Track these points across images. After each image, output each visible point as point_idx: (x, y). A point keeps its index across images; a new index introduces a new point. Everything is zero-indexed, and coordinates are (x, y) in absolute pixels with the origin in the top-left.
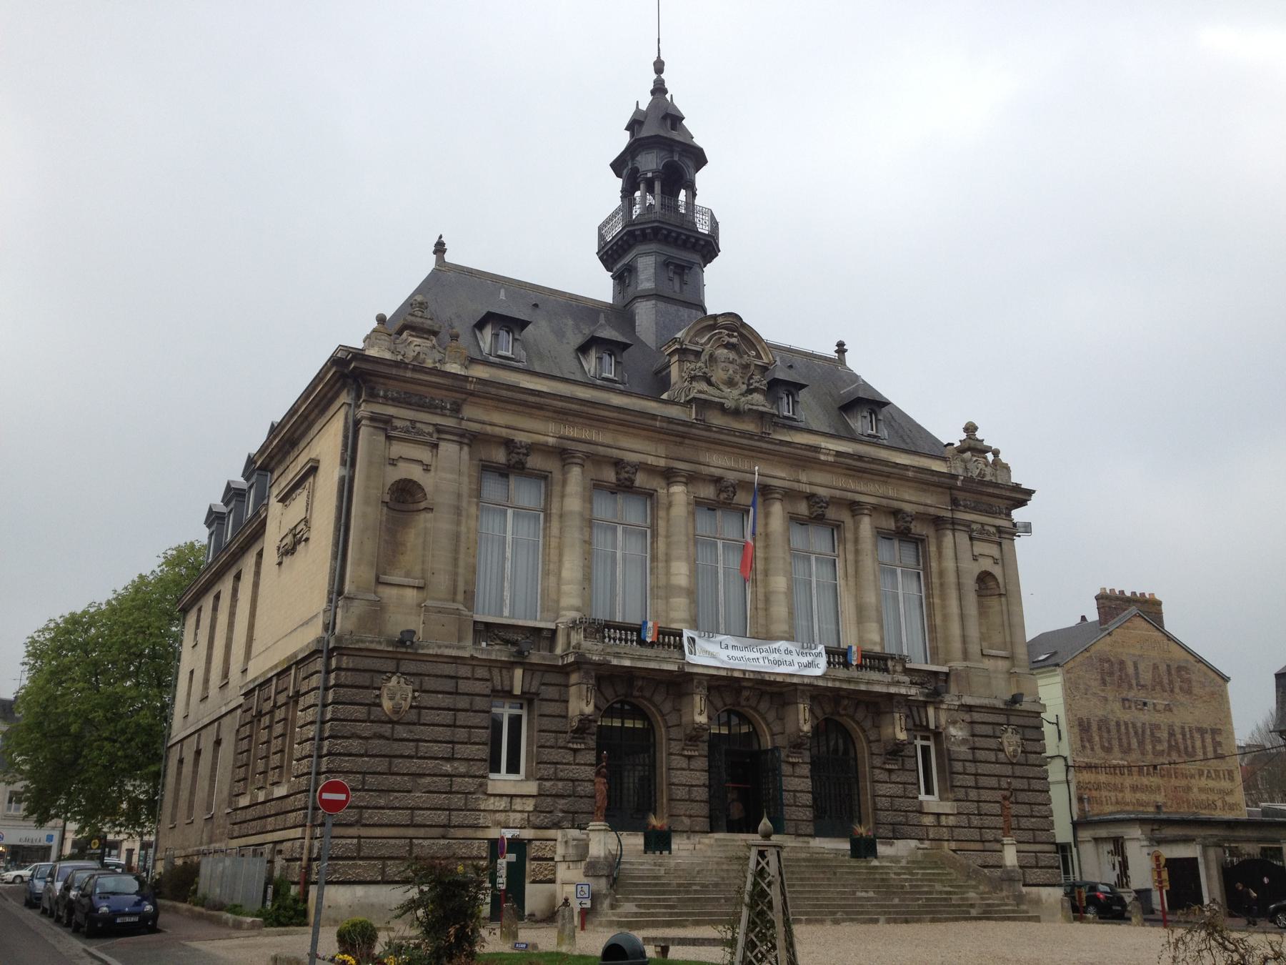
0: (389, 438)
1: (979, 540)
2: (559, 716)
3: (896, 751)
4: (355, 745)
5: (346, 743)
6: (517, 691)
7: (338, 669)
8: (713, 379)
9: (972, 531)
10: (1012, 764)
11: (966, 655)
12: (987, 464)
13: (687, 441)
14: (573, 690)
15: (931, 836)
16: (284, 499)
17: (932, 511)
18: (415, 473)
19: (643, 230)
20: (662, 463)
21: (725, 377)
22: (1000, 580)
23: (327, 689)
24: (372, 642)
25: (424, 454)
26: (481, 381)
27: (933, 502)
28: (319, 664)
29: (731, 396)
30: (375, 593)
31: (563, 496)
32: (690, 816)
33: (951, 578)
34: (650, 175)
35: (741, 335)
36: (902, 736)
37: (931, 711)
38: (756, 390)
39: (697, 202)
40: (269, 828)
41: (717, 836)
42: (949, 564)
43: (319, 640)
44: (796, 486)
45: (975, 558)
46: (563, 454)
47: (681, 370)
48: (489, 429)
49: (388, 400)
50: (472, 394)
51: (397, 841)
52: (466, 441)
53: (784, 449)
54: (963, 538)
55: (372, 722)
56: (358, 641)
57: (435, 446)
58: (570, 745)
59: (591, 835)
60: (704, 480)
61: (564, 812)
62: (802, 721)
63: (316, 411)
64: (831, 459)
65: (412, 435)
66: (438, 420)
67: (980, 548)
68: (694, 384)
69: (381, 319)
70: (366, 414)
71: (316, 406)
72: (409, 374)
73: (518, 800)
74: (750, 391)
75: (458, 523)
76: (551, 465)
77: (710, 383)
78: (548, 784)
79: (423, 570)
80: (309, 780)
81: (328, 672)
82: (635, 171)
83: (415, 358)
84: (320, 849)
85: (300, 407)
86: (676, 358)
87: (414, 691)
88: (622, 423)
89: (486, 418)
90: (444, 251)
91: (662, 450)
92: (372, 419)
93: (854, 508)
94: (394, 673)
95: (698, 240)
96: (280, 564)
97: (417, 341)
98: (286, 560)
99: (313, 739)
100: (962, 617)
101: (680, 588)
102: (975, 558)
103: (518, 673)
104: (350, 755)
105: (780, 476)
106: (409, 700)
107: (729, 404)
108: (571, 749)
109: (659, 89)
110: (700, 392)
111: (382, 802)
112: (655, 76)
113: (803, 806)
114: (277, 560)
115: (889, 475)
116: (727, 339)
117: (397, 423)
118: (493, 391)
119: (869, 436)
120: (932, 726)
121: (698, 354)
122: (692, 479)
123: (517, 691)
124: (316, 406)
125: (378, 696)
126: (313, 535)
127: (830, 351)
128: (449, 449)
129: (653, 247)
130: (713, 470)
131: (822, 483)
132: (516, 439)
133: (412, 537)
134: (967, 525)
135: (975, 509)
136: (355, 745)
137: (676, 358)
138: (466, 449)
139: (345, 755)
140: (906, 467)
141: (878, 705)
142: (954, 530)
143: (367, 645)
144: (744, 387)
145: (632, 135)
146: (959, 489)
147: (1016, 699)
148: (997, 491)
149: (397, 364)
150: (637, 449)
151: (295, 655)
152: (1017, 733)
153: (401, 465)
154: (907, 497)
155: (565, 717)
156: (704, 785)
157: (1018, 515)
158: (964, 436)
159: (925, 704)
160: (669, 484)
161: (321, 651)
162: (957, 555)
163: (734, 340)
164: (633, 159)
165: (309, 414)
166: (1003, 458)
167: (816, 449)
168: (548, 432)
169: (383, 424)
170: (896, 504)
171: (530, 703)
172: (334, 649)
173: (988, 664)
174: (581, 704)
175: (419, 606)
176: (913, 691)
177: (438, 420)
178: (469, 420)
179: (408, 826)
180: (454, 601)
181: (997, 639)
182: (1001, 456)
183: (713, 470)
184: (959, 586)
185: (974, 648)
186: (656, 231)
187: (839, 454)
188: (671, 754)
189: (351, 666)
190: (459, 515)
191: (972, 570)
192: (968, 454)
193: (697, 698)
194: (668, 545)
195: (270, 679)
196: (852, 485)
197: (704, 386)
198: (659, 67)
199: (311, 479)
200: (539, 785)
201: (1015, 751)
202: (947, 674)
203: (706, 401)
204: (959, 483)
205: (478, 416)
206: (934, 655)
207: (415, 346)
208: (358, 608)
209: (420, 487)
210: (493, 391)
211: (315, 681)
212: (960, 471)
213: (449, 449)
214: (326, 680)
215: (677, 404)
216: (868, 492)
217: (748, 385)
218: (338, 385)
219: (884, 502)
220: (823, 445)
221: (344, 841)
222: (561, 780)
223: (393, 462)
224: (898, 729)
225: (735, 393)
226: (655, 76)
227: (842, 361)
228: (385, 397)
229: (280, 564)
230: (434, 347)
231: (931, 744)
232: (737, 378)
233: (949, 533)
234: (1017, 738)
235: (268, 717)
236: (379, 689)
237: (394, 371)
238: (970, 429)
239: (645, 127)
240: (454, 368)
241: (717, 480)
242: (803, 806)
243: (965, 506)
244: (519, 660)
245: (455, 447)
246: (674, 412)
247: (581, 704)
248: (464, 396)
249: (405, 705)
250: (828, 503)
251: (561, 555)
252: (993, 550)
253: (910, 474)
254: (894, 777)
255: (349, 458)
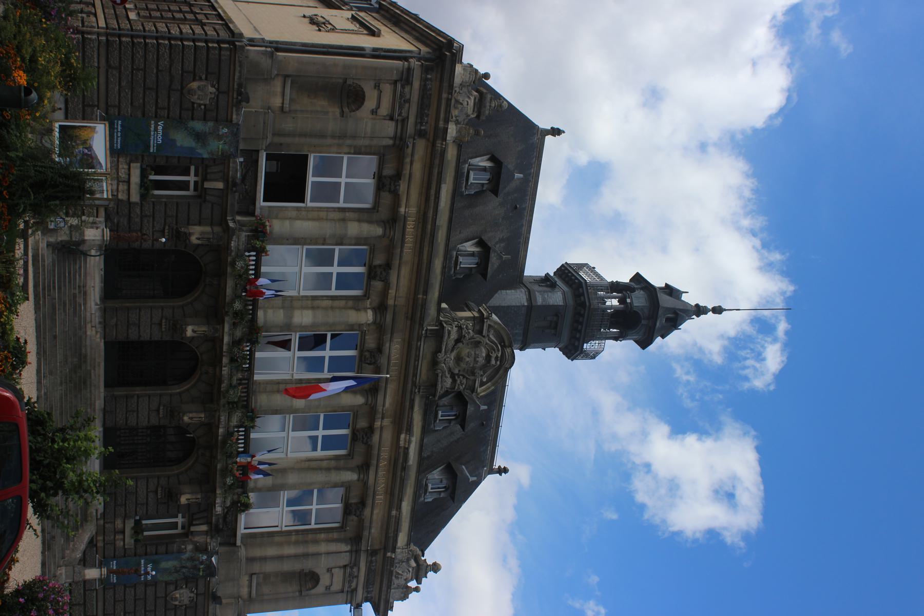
0: (395, 82)
1: (345, 573)
2: (189, 219)
3: (172, 496)
4: (165, 63)
5: (166, 56)
6: (207, 185)
7: (220, 49)
8: (460, 345)
9: (352, 568)
10: (166, 596)
11: (250, 560)
12: (407, 581)
13: (409, 322)
14: (208, 229)
15: (107, 526)
16: (354, 18)
17: (366, 533)
18: (370, 103)
19: (583, 294)
20: (391, 302)
21: (463, 354)
22: (313, 591)
23: (206, 41)
24: (240, 72)
25: (384, 110)
26: (443, 153)
27: (375, 531)
28: (224, 35)
29: (447, 360)
30: (277, 75)
31: (359, 221)
32: (116, 325)
33: (312, 549)
34: (628, 301)
35: (500, 367)
36: (183, 500)
37: (204, 528)
38: (454, 381)
39: (609, 342)
40: (106, 11)
41: (102, 344)
42: (323, 548)
43: (241, 35)
44: (379, 416)
45: (329, 570)
46: (393, 220)
47: (467, 319)
48: (408, 160)
49: (424, 81)
50: (434, 145)
51: (96, 96)
52: (397, 142)
53: (407, 404)
54: (345, 559)
55: (182, 75)
56: (240, 62)
57: (391, 118)
58: (159, 489)
59: (99, 230)
60: (379, 339)
61: (118, 223)
62: (191, 415)
63: (417, 35)
64: (402, 443)
65: (401, 101)
66: (412, 120)
67: (338, 574)
68: (455, 329)
69: (487, 76)
70: (412, 65)
71: (422, 35)
72: (445, 96)
73: (126, 187)
74: (453, 376)
75: (333, 137)
76: (384, 213)
77: (458, 341)
78: (138, 210)
79: (295, 111)
80: (140, 31)
81: (218, 42)
82: (632, 290)
83: (457, 101)
84: (90, 39)
85: (421, 24)
86: (476, 315)
87: (205, 105)
88: (419, 271)
89: (416, 157)
90: (554, 135)
91: (401, 301)
92: (409, 69)
93: (364, 468)
94: (218, 90)
95: (578, 340)
96: (304, 16)
97: (471, 103)
98: (307, 20)
99: (169, 32)
100: (281, 558)
101: (291, 317)
102: (329, 570)
103: (220, 185)
104: (158, 60)
105: (388, 400)
106: (199, 101)
107: (441, 356)
108: (164, 229)
109: (699, 311)
110: (449, 332)
111: (124, 84)
112: (710, 307)
113: (126, 418)
114: (307, 14)
115: (392, 495)
116: (494, 355)
117: (407, 89)
118: (437, 161)
119: (426, 485)
120: (193, 529)
121: (480, 332)
122: (379, 327)
123: (207, 185)
124: (422, 35)
125: (201, 79)
126: (322, 34)
127: (498, 462)
128: (390, 128)
129: (571, 302)
130: (388, 345)
131: (383, 437)
132: (401, 182)
133: (321, 103)
134: (355, 564)
135: (369, 570)
136: (165, 63)
137: (476, 315)
138: (391, 142)
139: (158, 55)
140: (399, 508)
141: (206, 483)
142: (351, 552)
143: (238, 68)
144: (456, 371)
145: (661, 288)
146: (385, 554)
147: (216, 599)
148: (384, 588)
149: (451, 86)
150: (401, 281)
151: (232, 22)
152: (191, 601)
153: (376, 93)
154: (376, 512)
155: (188, 224)
156: (140, 336)
157: (367, 608)
158: (430, 562)
159: (209, 523)
160: (374, 309)
161: (233, 37)
162: (330, 558)
163: (493, 362)
164: (642, 289)
165: (416, 31)
166: (413, 595)
167: (409, 431)
168: (409, 208)
169: (405, 78)
170: (369, 502)
171: (199, 197)
172: (235, 46)
173: (245, 580)
174: (197, 234)
175: (269, 108)
176: (219, 509)
177: (412, 120)
178: (414, 144)
179: (107, 103)
180: (274, 134)
181: (266, 590)
182: (414, 593)
183: (388, 345)
184: (306, 556)
185: (257, 567)
186: (583, 305)
187: (407, 449)
188: (162, 310)
189: (223, 58)
190: (340, 137)
191: (320, 566)
192: (413, 564)
193: (204, 328)
194: (326, 308)
195: (216, 10)
196: (383, 463)
197: (454, 336)
198: (718, 310)
199: (365, 32)
200: (136, 203)
201: (176, 599)
202: (234, 544)
203: (442, 337)
204: (389, 554)
205: (419, 150)
206: (251, 539)
207: (469, 103)
208: (265, 62)
209: (360, 107)
210: (437, 161)
211: (211, 32)
212: (399, 557)
213: (390, 128)
214: (213, 41)
215: (438, 315)
216: (379, 478)
217: (458, 375)
218: (435, 46)
219: (371, 492)
220: (414, 439)
221: (95, 56)
222: (142, 221)
223: (377, 86)
224: (188, 496)
225: (452, 364)
226: (710, 307)
227: (492, 471)
228: (426, 79)
229: (304, 16)
230: (468, 116)
231: (179, 531)
232: (463, 365)
233: (348, 548)
234: (186, 602)
235: (188, 9)
236: (206, 79)
237: (445, 84)
238: (435, 568)
239: (668, 298)
240: (452, 130)
241: (379, 349)
242: (126, 418)
243: (371, 562)
244: (230, 185)
245: (392, 135)
246: (432, 311)
247: (197, 234)
248: (431, 139)
249: (194, 99)
250: (366, 443)
251: (313, 219)
252: (337, 586)
253: (394, 513)
254: (151, 495)
255: (377, 53)
